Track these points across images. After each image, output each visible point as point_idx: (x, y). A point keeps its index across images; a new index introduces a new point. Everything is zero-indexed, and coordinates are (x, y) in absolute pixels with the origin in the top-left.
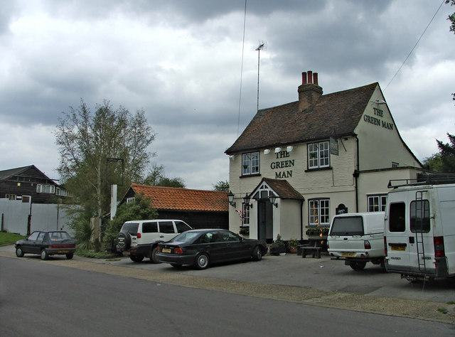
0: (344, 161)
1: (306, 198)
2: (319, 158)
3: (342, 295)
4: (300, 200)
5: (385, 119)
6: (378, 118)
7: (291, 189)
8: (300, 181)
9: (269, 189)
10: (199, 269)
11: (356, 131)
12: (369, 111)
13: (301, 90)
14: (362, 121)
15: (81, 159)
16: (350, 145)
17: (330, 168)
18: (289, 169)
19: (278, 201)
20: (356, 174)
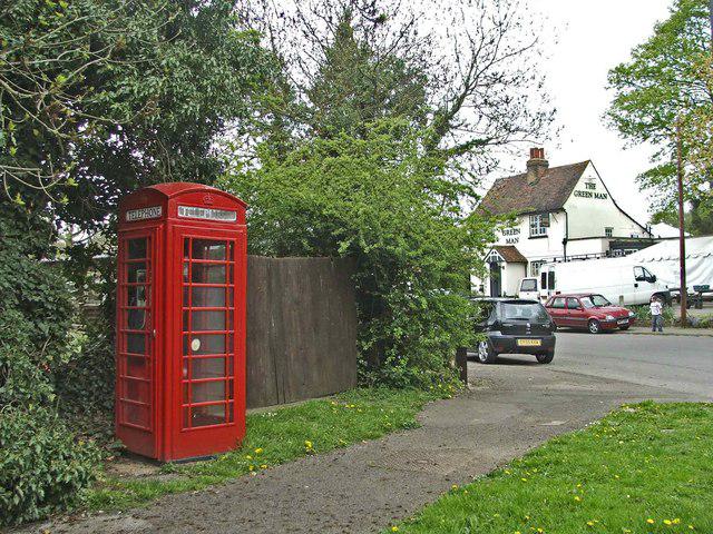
0: (556, 229)
1: (529, 260)
2: (538, 228)
3: (273, 281)
4: (524, 262)
5: (600, 190)
6: (590, 191)
7: (517, 253)
8: (529, 248)
9: (498, 255)
10: (590, 333)
11: (565, 207)
12: (580, 186)
13: (529, 165)
14: (572, 195)
15: (325, 58)
16: (561, 218)
17: (546, 237)
18: (516, 236)
19: (504, 264)
20: (565, 242)
